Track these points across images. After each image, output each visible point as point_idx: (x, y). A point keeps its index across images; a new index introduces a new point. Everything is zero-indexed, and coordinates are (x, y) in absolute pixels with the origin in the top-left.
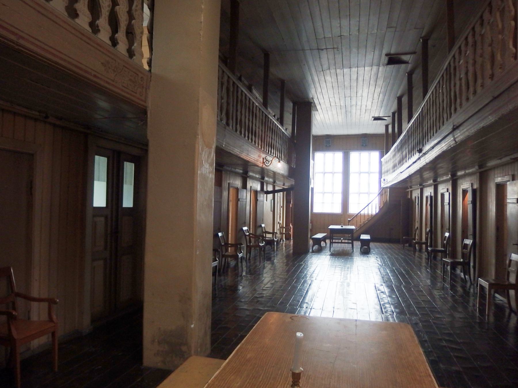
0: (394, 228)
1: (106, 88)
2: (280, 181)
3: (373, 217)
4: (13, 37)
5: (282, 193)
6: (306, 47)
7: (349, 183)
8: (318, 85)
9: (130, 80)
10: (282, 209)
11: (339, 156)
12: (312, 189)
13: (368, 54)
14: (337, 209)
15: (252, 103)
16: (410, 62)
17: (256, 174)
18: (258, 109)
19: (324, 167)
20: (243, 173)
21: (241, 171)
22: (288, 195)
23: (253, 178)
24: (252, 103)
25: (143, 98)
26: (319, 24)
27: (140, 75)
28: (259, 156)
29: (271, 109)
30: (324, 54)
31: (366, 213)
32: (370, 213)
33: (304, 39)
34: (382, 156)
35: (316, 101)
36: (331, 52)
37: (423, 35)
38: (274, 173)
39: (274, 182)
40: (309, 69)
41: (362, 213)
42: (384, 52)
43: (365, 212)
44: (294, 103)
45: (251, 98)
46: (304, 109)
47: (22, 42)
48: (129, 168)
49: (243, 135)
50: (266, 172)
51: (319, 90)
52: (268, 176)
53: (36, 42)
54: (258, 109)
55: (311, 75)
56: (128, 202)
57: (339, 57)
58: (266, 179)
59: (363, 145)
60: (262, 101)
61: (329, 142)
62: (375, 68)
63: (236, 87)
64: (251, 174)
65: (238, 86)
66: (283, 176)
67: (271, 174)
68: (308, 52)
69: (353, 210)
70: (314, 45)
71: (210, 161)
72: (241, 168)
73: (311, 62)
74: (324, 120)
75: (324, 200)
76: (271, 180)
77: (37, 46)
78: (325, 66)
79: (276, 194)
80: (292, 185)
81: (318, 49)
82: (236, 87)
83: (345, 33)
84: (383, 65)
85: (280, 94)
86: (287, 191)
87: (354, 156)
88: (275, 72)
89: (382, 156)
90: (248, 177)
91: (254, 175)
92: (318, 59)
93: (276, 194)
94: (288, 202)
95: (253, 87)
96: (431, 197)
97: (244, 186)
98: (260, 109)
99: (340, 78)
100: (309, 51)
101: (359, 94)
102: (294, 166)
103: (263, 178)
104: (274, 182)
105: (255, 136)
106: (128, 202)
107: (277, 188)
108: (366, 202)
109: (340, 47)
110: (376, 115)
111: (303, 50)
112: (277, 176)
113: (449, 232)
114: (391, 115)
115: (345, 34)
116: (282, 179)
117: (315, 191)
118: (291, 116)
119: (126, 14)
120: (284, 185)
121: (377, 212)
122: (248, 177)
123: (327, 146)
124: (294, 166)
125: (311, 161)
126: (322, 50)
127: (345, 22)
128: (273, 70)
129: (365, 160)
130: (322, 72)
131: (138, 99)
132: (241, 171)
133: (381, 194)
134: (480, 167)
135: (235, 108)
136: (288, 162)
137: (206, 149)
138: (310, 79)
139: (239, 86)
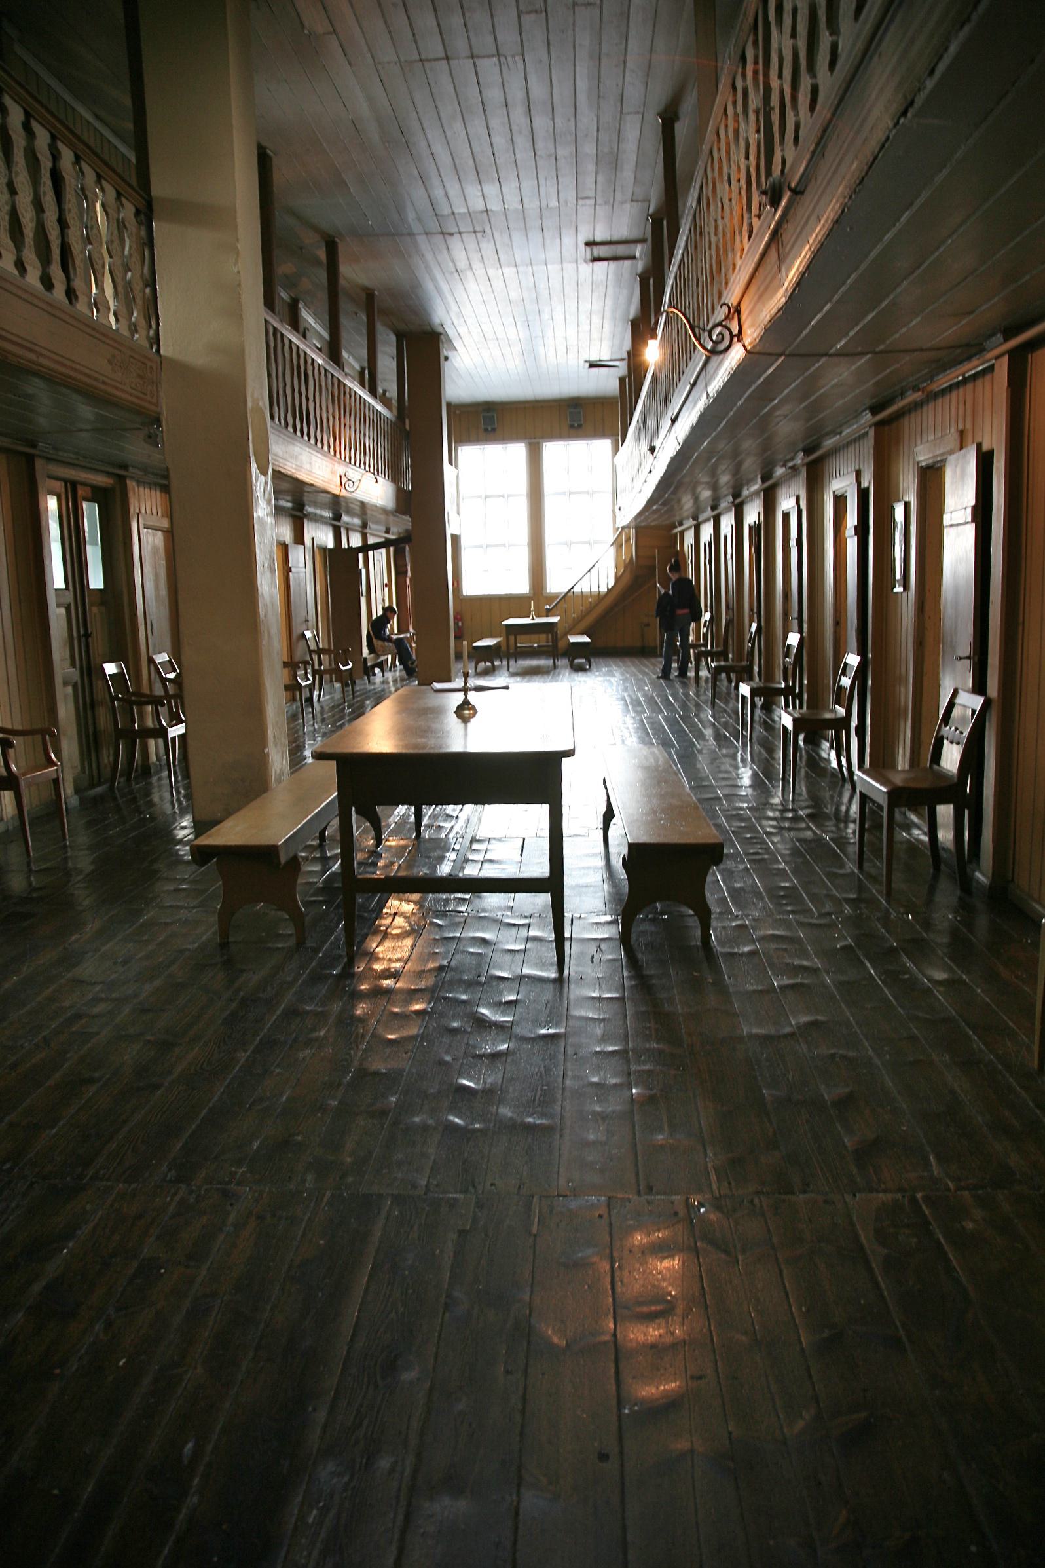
0: (647, 618)
1: (74, 379)
2: (377, 522)
3: (600, 598)
4: (33, 356)
5: (383, 551)
6: (416, 228)
7: (540, 521)
8: (450, 299)
9: (139, 376)
10: (386, 589)
11: (517, 452)
12: (456, 539)
13: (548, 242)
14: (521, 586)
15: (310, 361)
16: (638, 255)
17: (321, 508)
18: (323, 371)
19: (481, 484)
20: (293, 509)
21: (289, 505)
22: (399, 555)
23: (316, 519)
24: (310, 361)
25: (154, 401)
26: (438, 193)
27: (149, 364)
28: (333, 472)
29: (350, 353)
30: (455, 243)
31: (586, 590)
32: (595, 589)
33: (411, 216)
34: (616, 450)
35: (451, 332)
36: (470, 240)
37: (651, 210)
38: (363, 505)
39: (365, 525)
40: (427, 267)
41: (577, 590)
42: (582, 239)
43: (583, 587)
44: (400, 336)
45: (308, 351)
46: (424, 348)
47: (42, 360)
48: (90, 513)
49: (298, 433)
50: (343, 504)
51: (454, 307)
52: (349, 512)
53: (66, 362)
54: (323, 371)
55: (433, 279)
56: (96, 581)
57: (487, 247)
58: (345, 518)
59: (572, 426)
60: (326, 335)
61: (490, 420)
62: (570, 267)
63: (279, 336)
64: (309, 509)
65: (282, 335)
66: (384, 511)
67: (357, 509)
68: (421, 239)
69: (556, 584)
70: (433, 226)
71: (267, 496)
72: (289, 498)
73: (429, 256)
74: (485, 352)
75: (488, 563)
76: (357, 521)
77: (85, 374)
78: (462, 263)
79: (370, 553)
80: (407, 531)
81: (443, 233)
82: (279, 336)
83: (495, 206)
84: (585, 261)
85: (364, 318)
86: (397, 546)
87: (554, 451)
88: (352, 272)
89: (616, 450)
90: (307, 516)
91: (318, 512)
92: (445, 252)
93: (370, 553)
94: (401, 573)
95: (301, 305)
96: (710, 543)
97: (299, 539)
98: (326, 370)
99: (498, 284)
100: (424, 237)
101: (546, 316)
102: (407, 485)
103: (338, 517)
104: (365, 525)
105: (322, 431)
106: (96, 581)
107: (371, 541)
108: (587, 564)
109: (488, 230)
110: (594, 358)
111: (411, 234)
112: (369, 512)
113: (801, 631)
114: (625, 356)
115: (494, 208)
116: (383, 517)
117: (464, 543)
118: (394, 365)
119: (70, 221)
120: (387, 531)
121: (611, 584)
122: (306, 516)
123: (486, 430)
124: (407, 485)
125: (448, 471)
126: (452, 234)
127: (491, 190)
128: (347, 270)
129: (573, 460)
130: (456, 275)
131: (150, 402)
132: (289, 505)
133: (618, 543)
134: (764, 480)
135: (280, 379)
136: (395, 476)
137: (262, 478)
138: (434, 293)
139: (285, 332)
